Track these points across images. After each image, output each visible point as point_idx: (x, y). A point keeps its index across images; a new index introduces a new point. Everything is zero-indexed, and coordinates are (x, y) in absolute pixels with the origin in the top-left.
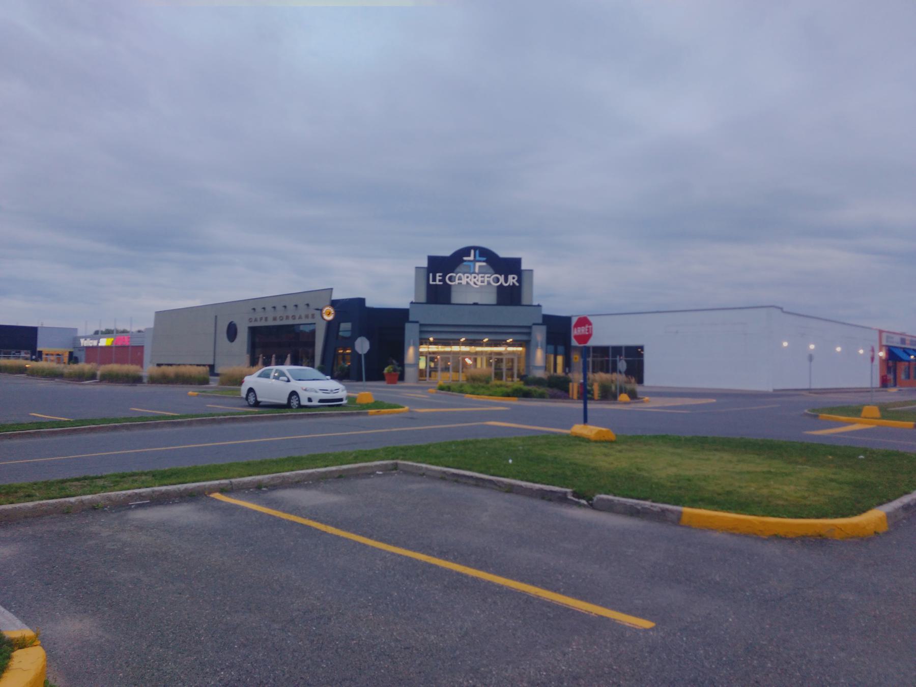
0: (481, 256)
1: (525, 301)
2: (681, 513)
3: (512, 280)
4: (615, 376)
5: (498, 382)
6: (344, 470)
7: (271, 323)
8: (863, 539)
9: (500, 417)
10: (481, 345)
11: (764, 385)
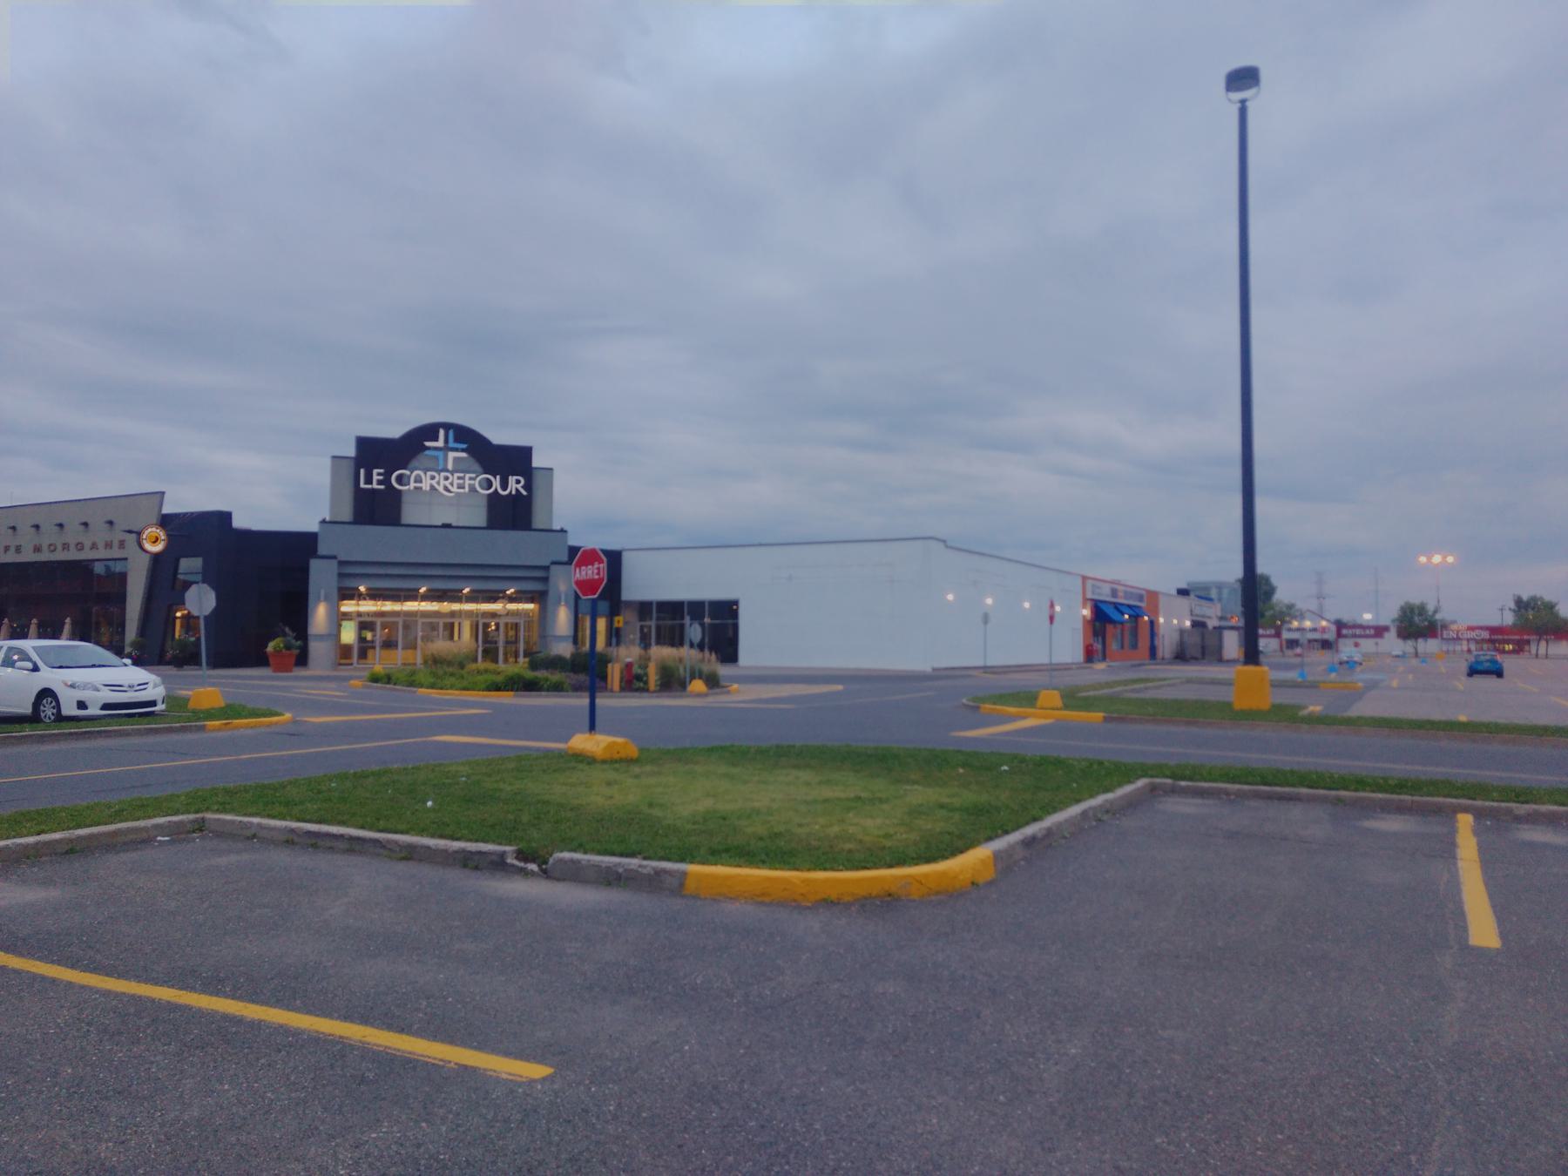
1: (539, 521)
2: (684, 874)
3: (515, 484)
4: (685, 652)
5: (491, 666)
6: (80, 838)
7: (28, 556)
8: (949, 895)
9: (465, 725)
10: (458, 599)
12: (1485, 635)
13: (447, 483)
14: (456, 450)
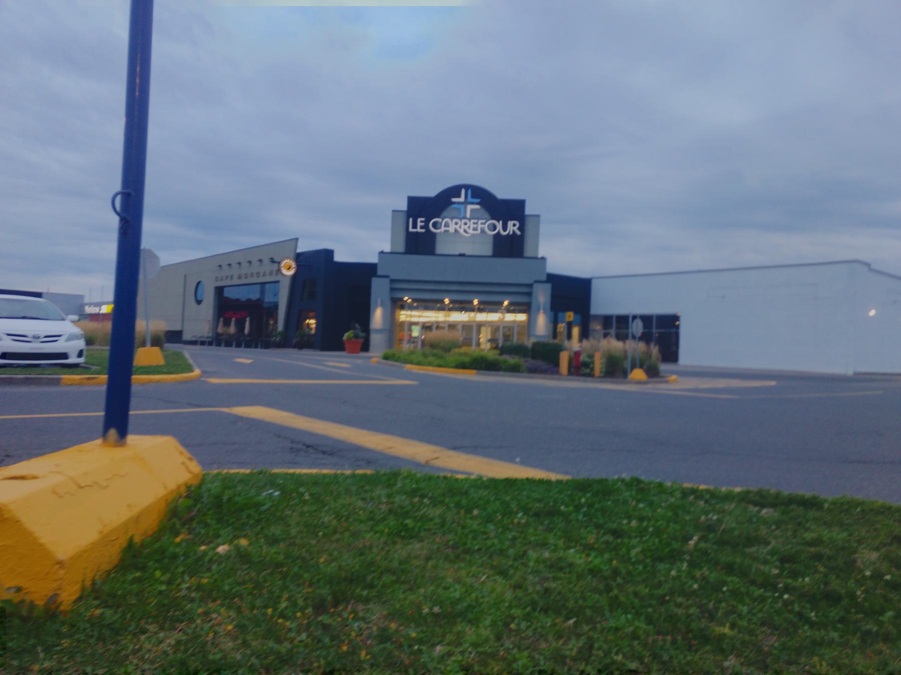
0: (473, 197)
1: (528, 252)
3: (513, 227)
13: (466, 227)
14: (472, 203)
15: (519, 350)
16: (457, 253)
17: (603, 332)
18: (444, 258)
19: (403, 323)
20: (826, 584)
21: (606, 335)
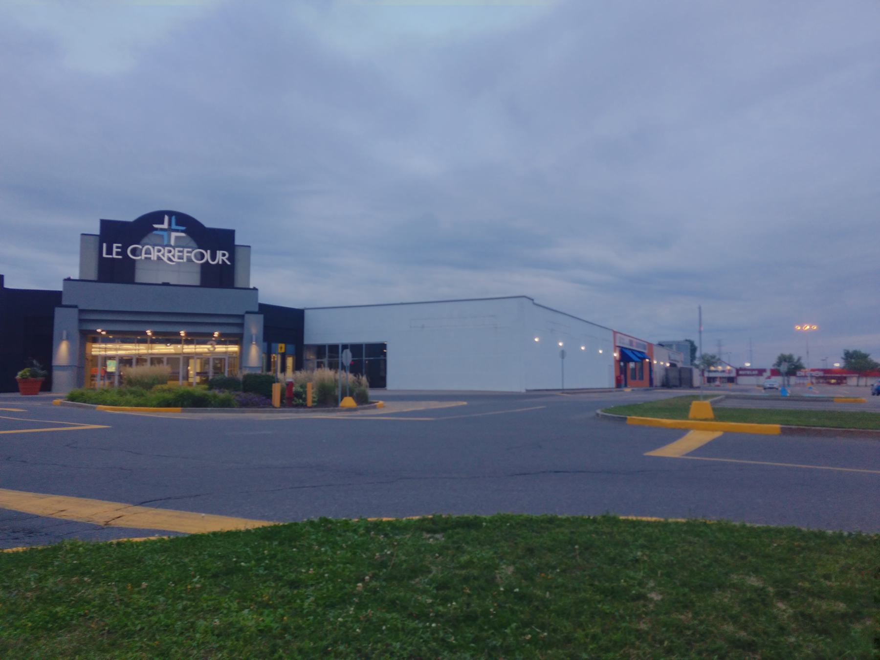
0: (177, 224)
1: (239, 283)
3: (221, 257)
10: (178, 342)
11: (517, 386)
12: (821, 374)
13: (170, 255)
14: (177, 231)
15: (229, 384)
16: (160, 282)
17: (316, 361)
18: (149, 287)
19: (96, 357)
20: (468, 605)
21: (319, 365)
